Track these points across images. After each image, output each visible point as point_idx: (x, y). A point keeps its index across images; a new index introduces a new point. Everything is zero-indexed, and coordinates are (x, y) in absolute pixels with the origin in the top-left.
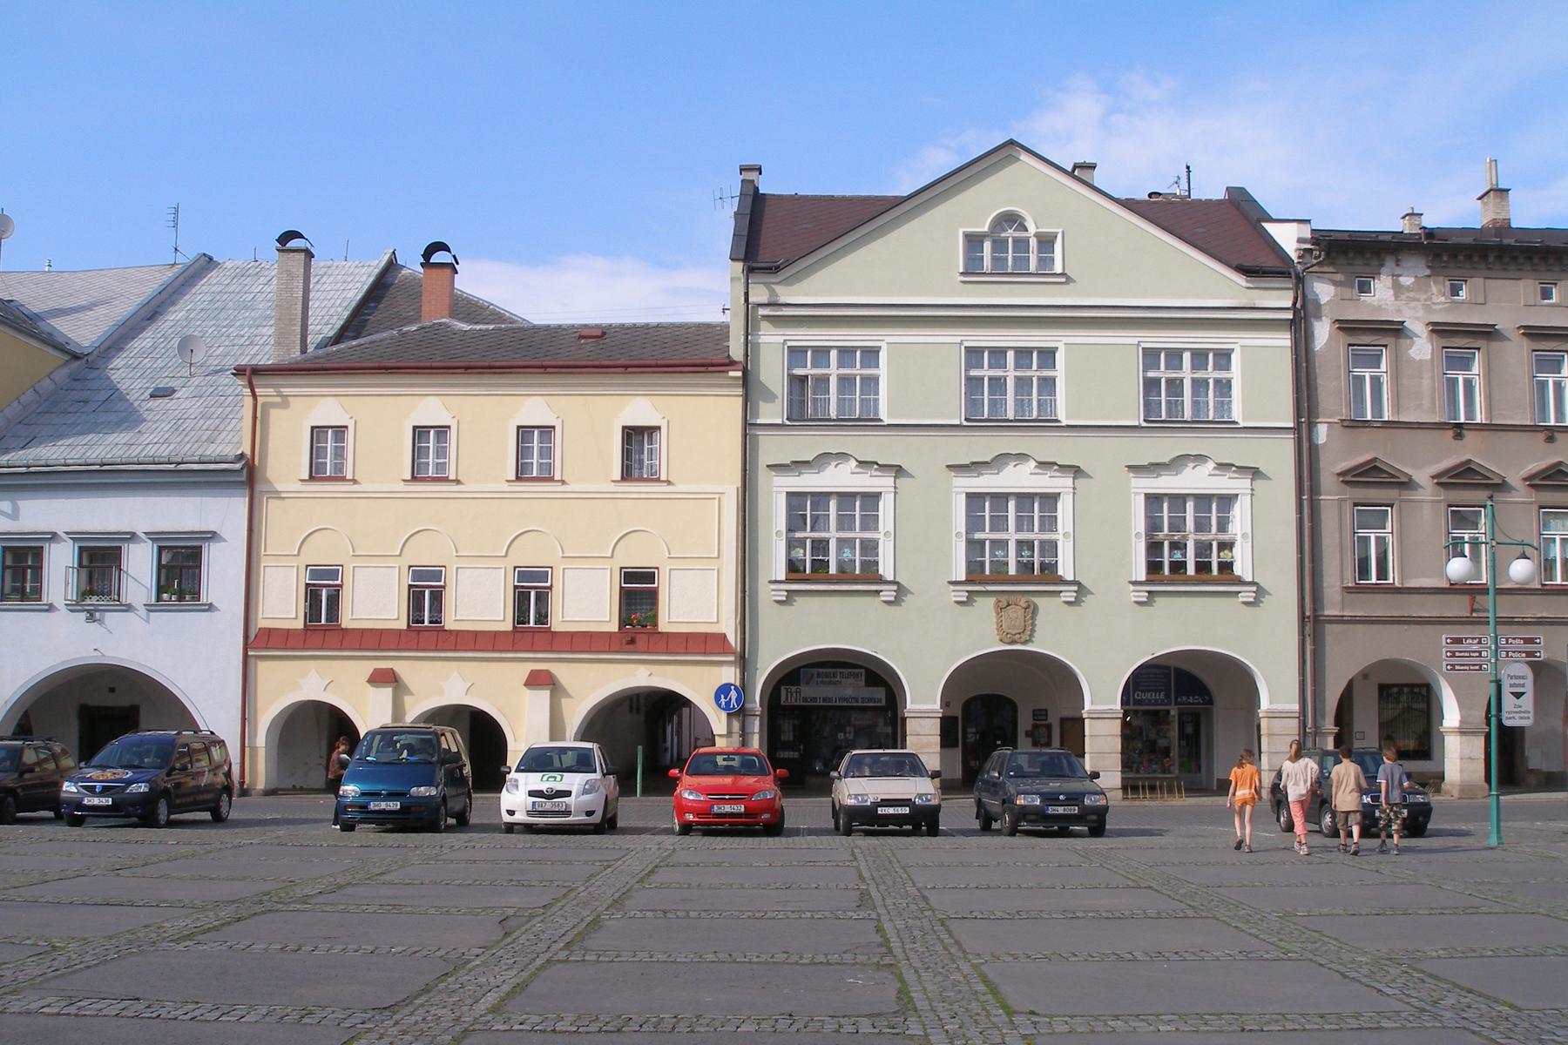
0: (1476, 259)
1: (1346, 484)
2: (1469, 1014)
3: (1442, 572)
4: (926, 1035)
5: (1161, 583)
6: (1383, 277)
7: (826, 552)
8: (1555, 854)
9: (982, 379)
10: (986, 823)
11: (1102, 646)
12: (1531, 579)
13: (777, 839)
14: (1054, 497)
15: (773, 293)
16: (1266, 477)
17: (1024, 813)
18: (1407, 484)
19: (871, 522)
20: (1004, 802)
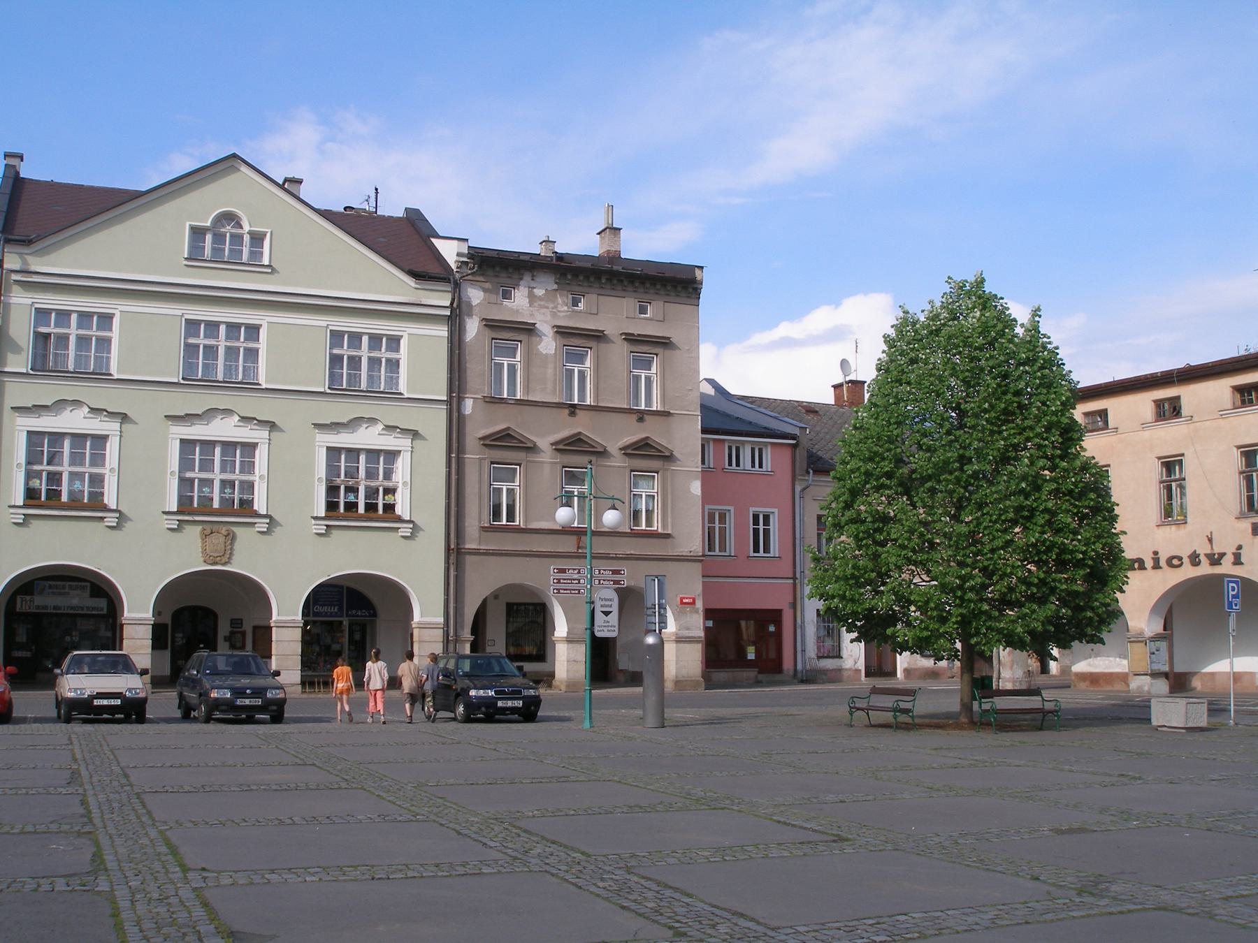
0: (592, 279)
1: (484, 445)
2: (551, 860)
3: (552, 518)
4: (112, 890)
5: (337, 519)
6: (521, 288)
7: (59, 483)
8: (631, 734)
9: (198, 346)
10: (187, 713)
11: (288, 569)
12: (620, 524)
13: (5, 726)
14: (253, 446)
15: (25, 262)
16: (424, 439)
17: (217, 704)
18: (532, 449)
19: (99, 459)
20: (201, 695)
